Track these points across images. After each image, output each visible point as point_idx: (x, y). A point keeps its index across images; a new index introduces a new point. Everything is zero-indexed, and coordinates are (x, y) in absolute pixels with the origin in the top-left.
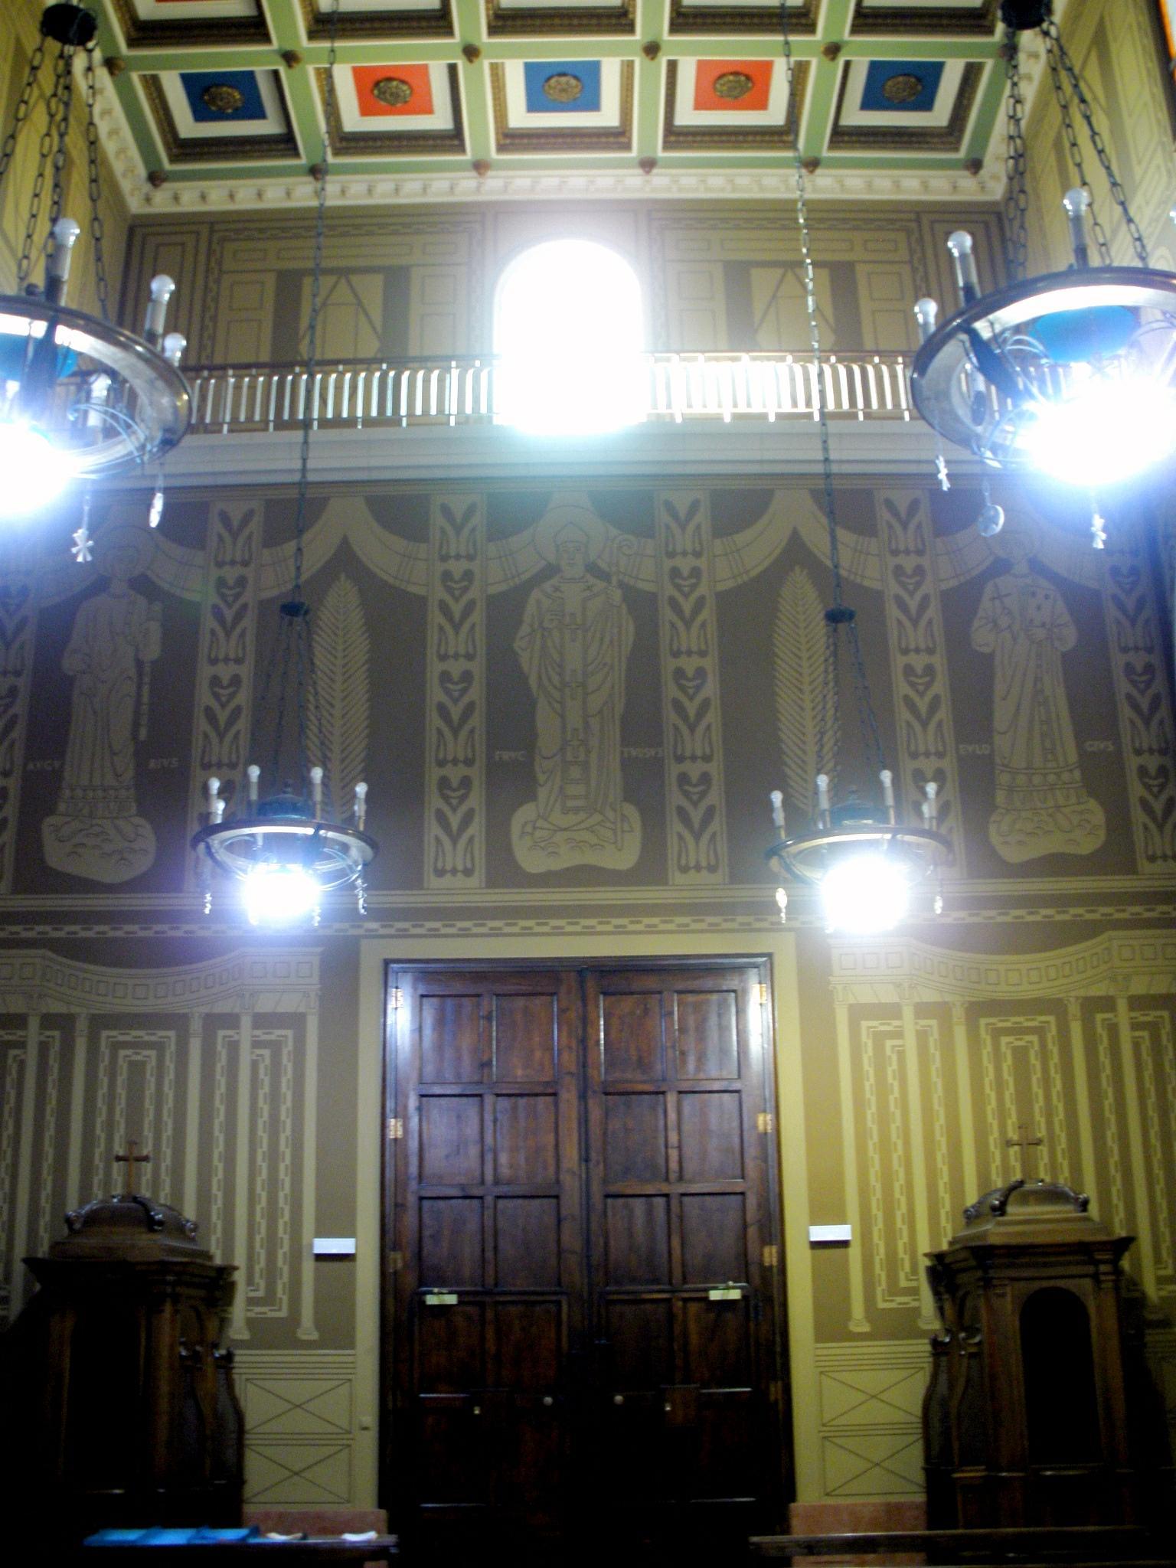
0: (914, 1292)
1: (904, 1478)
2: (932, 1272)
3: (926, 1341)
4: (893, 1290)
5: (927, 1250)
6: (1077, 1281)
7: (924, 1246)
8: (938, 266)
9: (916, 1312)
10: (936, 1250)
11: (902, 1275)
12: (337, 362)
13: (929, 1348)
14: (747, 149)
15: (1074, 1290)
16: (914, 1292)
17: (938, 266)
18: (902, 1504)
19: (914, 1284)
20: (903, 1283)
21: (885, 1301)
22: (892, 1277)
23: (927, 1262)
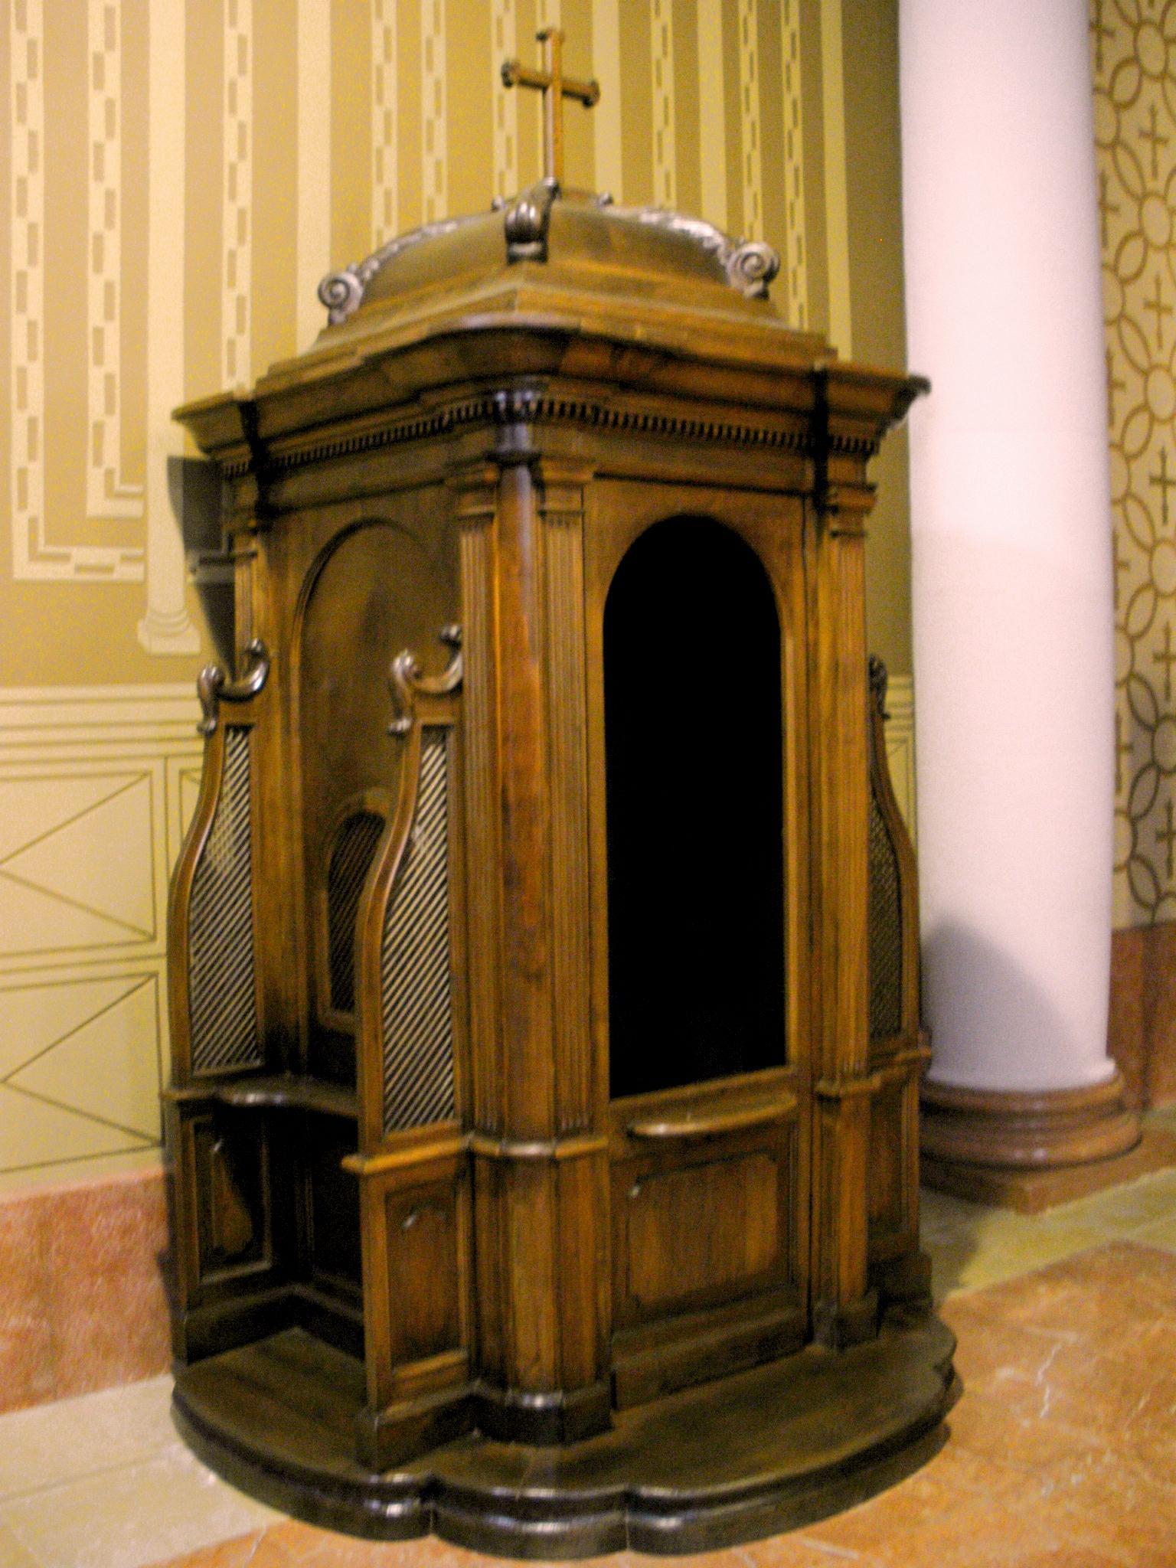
0: (128, 533)
1: (89, 910)
2: (201, 486)
3: (192, 689)
4: (66, 522)
5: (178, 399)
6: (742, 499)
7: (170, 387)
8: (120, 960)
9: (135, 596)
10: (207, 391)
11: (95, 479)
12: (507, 375)
13: (196, 711)
14: (380, 844)
15: (735, 520)
16: (128, 533)
17: (120, 960)
18: (85, 1196)
19: (133, 508)
20: (97, 504)
21: (35, 556)
22: (64, 485)
23: (181, 443)
